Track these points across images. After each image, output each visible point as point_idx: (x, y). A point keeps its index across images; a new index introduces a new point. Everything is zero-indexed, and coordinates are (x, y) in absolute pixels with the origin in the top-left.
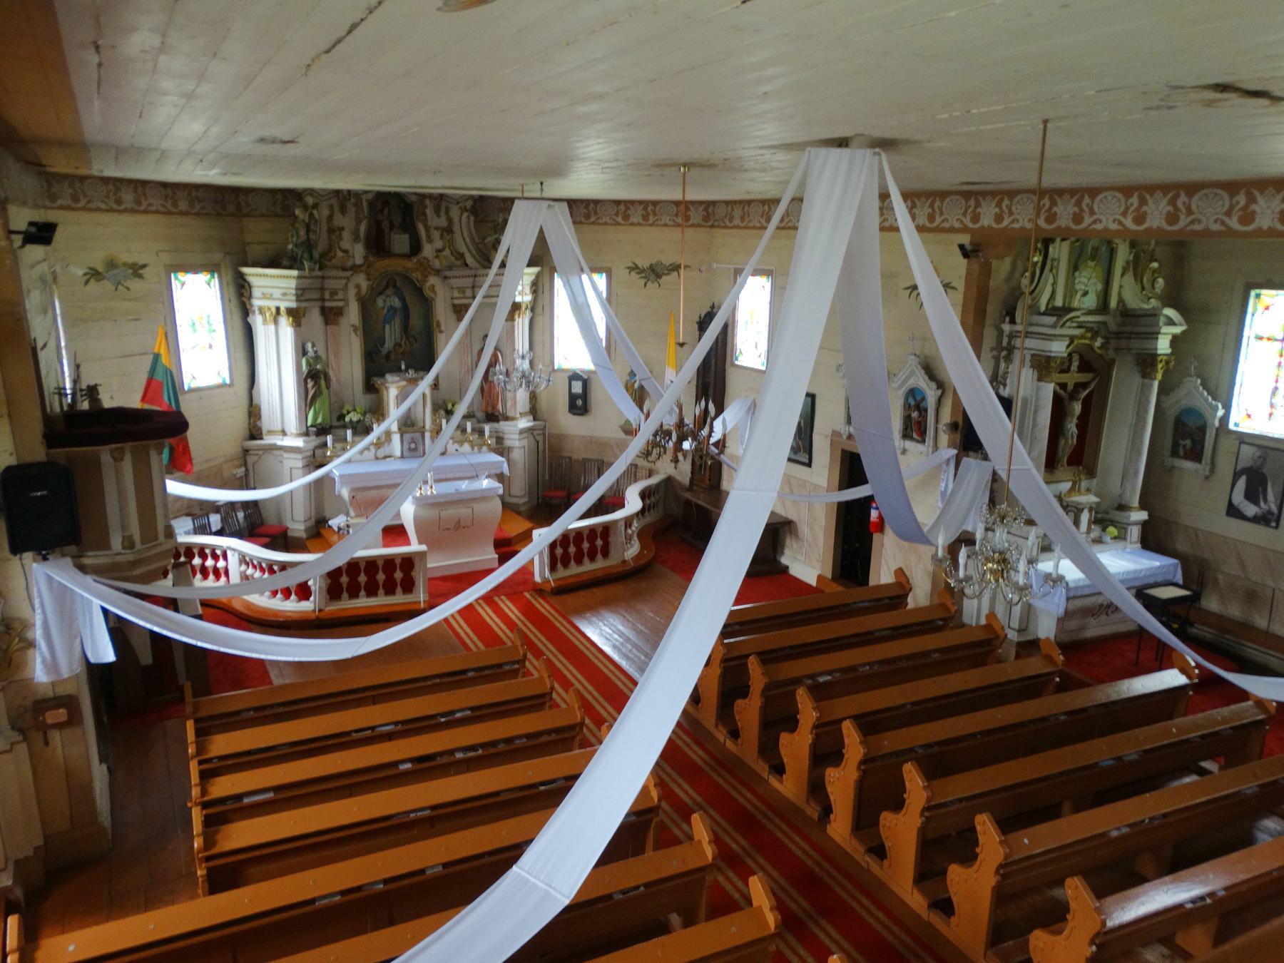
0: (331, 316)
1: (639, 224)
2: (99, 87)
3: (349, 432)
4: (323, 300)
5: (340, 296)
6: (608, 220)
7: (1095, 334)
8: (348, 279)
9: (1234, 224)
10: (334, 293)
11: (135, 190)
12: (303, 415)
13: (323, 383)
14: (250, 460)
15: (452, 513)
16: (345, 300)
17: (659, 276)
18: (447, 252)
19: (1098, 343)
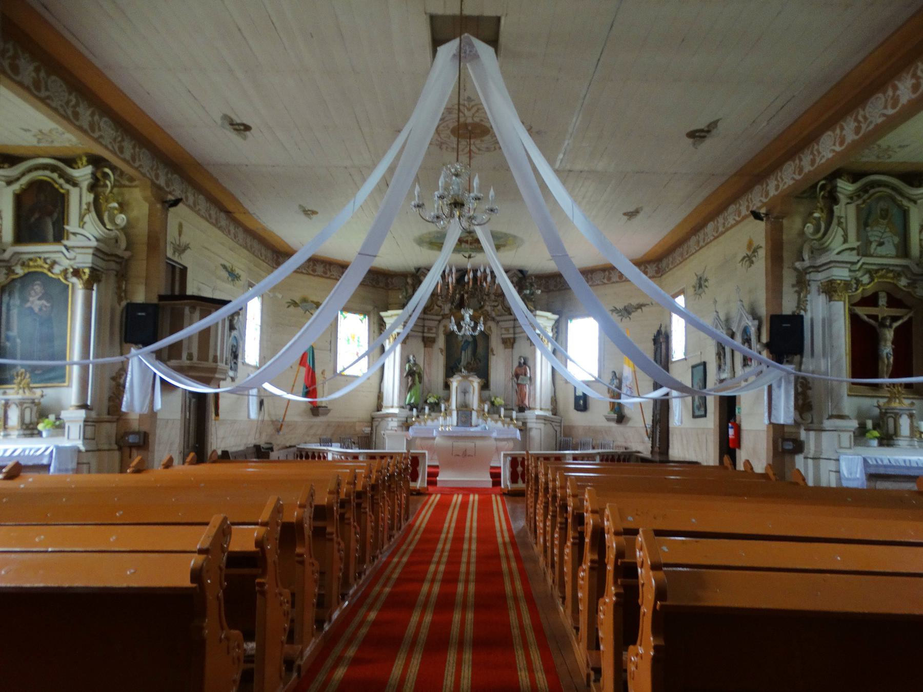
0: (428, 342)
1: (617, 282)
2: (46, 8)
3: (427, 408)
4: (423, 332)
5: (434, 330)
6: (599, 282)
7: (898, 275)
8: (440, 321)
9: (890, 112)
10: (430, 329)
11: (325, 267)
12: (402, 396)
13: (417, 379)
14: (375, 424)
15: (461, 444)
16: (437, 333)
17: (629, 313)
18: (500, 307)
19: (903, 282)
